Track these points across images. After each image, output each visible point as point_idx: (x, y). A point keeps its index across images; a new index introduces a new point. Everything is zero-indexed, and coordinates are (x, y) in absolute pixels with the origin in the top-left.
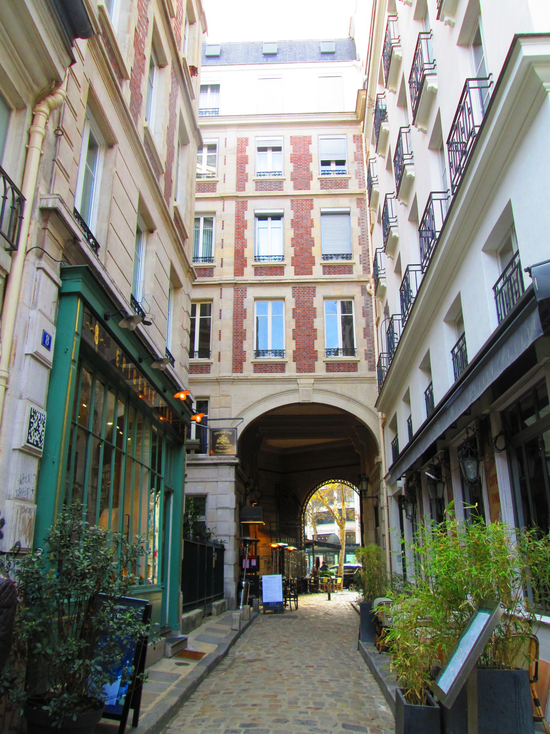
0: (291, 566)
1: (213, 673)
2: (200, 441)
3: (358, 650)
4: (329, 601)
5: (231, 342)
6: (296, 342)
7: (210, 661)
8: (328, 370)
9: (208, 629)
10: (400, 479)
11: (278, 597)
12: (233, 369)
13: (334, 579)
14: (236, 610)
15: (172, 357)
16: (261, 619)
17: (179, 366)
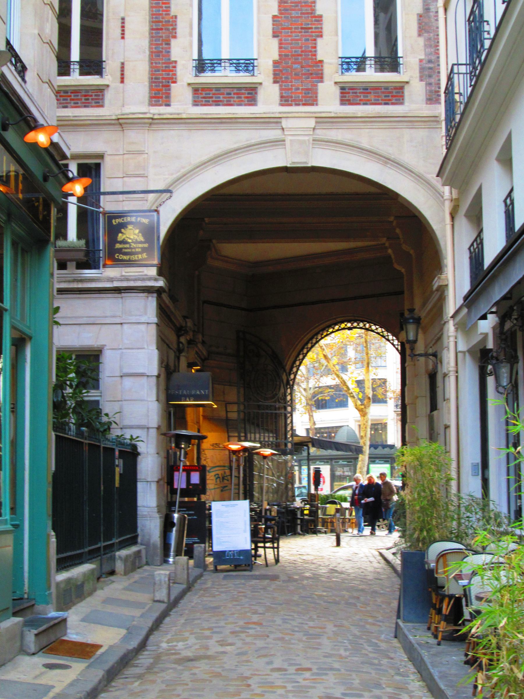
0: (265, 485)
1: (118, 682)
2: (87, 243)
3: (396, 637)
4: (338, 548)
5: (145, 43)
6: (280, 44)
7: (112, 660)
8: (344, 101)
9: (107, 601)
10: (484, 317)
11: (244, 542)
12: (151, 97)
13: (346, 509)
14: (161, 565)
15: (21, 62)
16: (210, 580)
17: (36, 81)
